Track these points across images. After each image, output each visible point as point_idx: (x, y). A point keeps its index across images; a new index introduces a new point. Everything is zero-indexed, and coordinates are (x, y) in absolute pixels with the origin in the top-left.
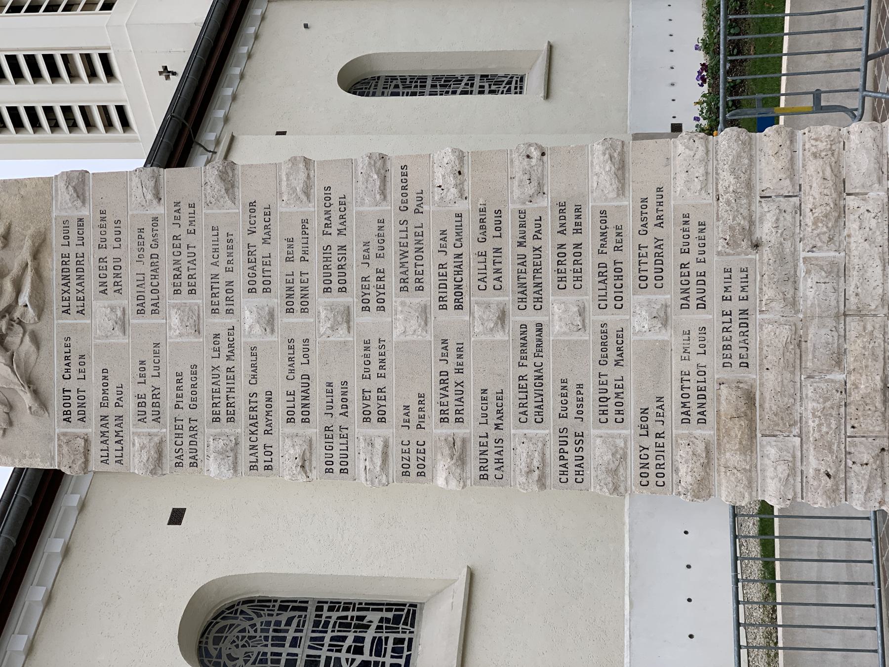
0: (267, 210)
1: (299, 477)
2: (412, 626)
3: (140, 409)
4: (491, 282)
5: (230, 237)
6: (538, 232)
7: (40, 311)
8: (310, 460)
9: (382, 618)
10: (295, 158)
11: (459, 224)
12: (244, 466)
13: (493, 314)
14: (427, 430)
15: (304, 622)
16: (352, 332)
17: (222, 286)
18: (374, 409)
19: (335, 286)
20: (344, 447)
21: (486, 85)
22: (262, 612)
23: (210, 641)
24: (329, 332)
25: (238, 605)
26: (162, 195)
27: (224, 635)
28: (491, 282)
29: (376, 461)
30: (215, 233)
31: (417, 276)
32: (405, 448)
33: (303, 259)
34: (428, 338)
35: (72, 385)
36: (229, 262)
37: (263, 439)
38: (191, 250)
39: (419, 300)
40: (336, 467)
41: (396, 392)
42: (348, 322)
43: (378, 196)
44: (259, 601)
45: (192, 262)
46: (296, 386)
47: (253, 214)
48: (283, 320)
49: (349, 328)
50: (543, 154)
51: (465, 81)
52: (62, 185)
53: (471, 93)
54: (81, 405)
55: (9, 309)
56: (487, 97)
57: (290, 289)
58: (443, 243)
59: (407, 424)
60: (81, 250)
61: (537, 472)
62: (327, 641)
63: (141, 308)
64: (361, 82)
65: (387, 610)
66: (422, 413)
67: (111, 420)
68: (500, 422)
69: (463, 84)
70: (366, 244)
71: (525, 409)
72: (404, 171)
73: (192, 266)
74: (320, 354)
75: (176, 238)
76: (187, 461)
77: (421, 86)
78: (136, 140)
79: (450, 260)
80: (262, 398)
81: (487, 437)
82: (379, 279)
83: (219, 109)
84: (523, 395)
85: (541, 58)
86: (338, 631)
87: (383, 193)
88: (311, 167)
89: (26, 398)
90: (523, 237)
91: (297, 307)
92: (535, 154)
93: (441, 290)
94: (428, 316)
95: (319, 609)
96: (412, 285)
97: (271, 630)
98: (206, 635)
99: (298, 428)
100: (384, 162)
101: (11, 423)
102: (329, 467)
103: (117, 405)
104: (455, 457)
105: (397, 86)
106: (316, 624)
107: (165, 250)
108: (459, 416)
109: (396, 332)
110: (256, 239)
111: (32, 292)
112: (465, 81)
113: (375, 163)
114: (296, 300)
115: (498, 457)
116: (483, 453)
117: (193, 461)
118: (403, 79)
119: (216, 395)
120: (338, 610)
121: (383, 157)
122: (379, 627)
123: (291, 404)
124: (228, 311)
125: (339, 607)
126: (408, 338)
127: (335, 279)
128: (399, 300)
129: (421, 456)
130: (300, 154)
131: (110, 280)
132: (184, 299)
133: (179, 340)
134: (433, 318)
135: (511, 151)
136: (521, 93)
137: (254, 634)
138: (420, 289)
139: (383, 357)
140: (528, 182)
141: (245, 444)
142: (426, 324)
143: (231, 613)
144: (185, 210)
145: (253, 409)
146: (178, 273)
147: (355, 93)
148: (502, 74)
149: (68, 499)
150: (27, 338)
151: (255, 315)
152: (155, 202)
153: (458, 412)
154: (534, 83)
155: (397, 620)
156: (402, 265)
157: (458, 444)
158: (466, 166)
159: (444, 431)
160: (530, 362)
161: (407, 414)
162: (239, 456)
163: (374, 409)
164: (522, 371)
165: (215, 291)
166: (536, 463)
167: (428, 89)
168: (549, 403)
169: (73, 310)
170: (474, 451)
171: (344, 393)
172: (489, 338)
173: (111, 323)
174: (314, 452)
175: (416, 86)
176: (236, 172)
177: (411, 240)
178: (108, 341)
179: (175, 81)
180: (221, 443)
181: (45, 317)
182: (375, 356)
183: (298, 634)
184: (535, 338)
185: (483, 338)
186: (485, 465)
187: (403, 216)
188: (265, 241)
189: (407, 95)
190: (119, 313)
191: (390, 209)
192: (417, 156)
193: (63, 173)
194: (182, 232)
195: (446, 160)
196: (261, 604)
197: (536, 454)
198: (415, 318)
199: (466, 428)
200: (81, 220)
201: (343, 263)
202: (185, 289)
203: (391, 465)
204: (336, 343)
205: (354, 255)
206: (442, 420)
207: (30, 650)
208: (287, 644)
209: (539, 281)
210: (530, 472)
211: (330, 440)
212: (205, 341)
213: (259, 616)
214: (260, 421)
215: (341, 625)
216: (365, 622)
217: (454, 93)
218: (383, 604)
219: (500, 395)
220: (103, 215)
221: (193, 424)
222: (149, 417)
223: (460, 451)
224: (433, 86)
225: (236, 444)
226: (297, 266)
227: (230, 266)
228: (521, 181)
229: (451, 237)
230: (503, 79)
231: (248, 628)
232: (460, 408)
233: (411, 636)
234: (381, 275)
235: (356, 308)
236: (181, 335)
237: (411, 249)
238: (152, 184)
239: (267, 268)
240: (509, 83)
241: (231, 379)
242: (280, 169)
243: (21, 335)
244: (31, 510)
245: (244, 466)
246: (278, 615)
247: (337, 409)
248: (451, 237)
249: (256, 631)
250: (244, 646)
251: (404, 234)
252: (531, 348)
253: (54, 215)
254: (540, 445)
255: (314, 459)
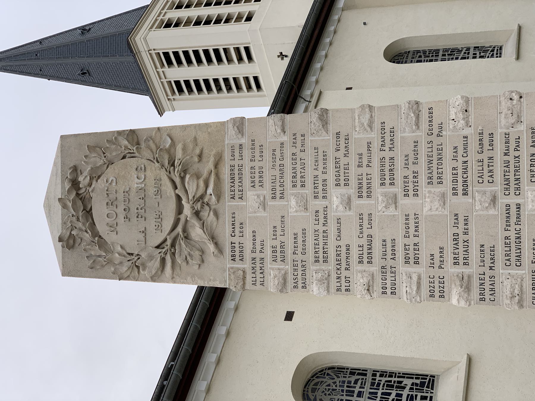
0: (347, 137)
1: (366, 296)
2: (432, 389)
3: (274, 254)
4: (486, 178)
5: (325, 153)
6: (518, 146)
7: (219, 197)
8: (373, 286)
9: (413, 383)
10: (363, 105)
11: (465, 142)
12: (333, 289)
13: (488, 198)
14: (445, 269)
15: (365, 382)
16: (398, 209)
17: (320, 182)
18: (411, 256)
19: (387, 182)
20: (393, 279)
21: (478, 53)
22: (340, 375)
23: (310, 390)
24: (384, 209)
25: (326, 370)
26: (286, 130)
27: (318, 387)
28: (486, 178)
29: (413, 287)
30: (316, 151)
31: (439, 175)
32: (431, 280)
33: (368, 166)
34: (446, 213)
35: (236, 240)
36: (324, 168)
37: (344, 273)
38: (302, 161)
39: (440, 189)
40: (389, 291)
41: (426, 245)
42: (396, 203)
43: (414, 127)
44: (338, 368)
45: (303, 168)
46: (364, 241)
47: (339, 140)
48: (356, 202)
49: (396, 206)
50: (521, 97)
51: (464, 51)
52: (230, 125)
53: (468, 58)
54: (241, 252)
55: (202, 197)
56: (478, 60)
57: (360, 183)
58: (455, 154)
59: (433, 265)
60: (241, 162)
61: (517, 297)
62: (379, 395)
63: (274, 195)
64: (397, 55)
65: (416, 378)
66: (442, 259)
67: (258, 260)
68: (493, 265)
69: (463, 53)
70: (407, 156)
71: (509, 257)
72: (431, 111)
73: (303, 171)
74: (378, 223)
75: (294, 154)
76: (300, 285)
77: (436, 56)
78: (265, 96)
79: (460, 165)
80: (344, 249)
81: (484, 274)
82: (415, 177)
83: (313, 76)
84: (508, 249)
85: (513, 34)
86: (386, 389)
87: (417, 125)
88: (373, 111)
89: (211, 247)
90: (508, 150)
91: (365, 194)
92: (516, 97)
93: (454, 183)
94: (446, 199)
95: (374, 375)
96: (435, 180)
97: (345, 386)
98: (307, 387)
99: (365, 267)
100: (418, 106)
101: (203, 261)
102: (384, 290)
103: (261, 252)
104: (463, 287)
105: (420, 57)
106: (373, 384)
107: (288, 162)
108: (466, 261)
109: (425, 209)
110: (340, 154)
111: (214, 187)
112: (464, 51)
113: (412, 107)
114: (364, 190)
115: (492, 287)
116: (481, 284)
117: (303, 285)
118: (424, 52)
119: (317, 247)
120: (386, 377)
121: (417, 103)
122: (411, 389)
123: (361, 252)
124: (324, 197)
125: (386, 375)
126: (433, 213)
127: (388, 178)
128: (427, 190)
129: (442, 285)
130: (366, 102)
131: (257, 179)
132: (298, 190)
133: (295, 214)
134: (449, 201)
135: (500, 96)
136: (500, 57)
137: (335, 388)
138: (440, 183)
139: (417, 225)
140: (511, 115)
141: (334, 276)
142: (444, 204)
143: (322, 374)
144: (299, 138)
145: (338, 255)
146: (295, 175)
147: (394, 62)
148: (488, 45)
149: (229, 304)
150: (212, 213)
151: (339, 200)
152: (282, 134)
153: (465, 258)
154: (509, 50)
155: (422, 384)
156: (429, 168)
157: (466, 278)
158: (470, 107)
159: (456, 270)
160: (513, 227)
161: (432, 259)
162: (330, 283)
163: (411, 256)
164: (507, 234)
165: (316, 185)
166: (517, 292)
167: (440, 57)
168: (525, 254)
169: (237, 197)
170: (475, 283)
171: (393, 246)
172: (485, 213)
173: (257, 205)
174: (375, 281)
175: (432, 56)
176: (328, 115)
177: (435, 153)
178: (255, 215)
179: (287, 61)
180: (320, 275)
181: (221, 201)
182: (412, 224)
183: (361, 390)
184: (515, 213)
185: (481, 213)
186: (483, 292)
187: (430, 138)
188: (345, 155)
189: (427, 62)
190: (262, 199)
191: (422, 134)
192: (439, 101)
193: (231, 119)
194: (297, 151)
195: (457, 103)
196: (339, 370)
197: (517, 286)
198: (437, 201)
199: (470, 268)
200: (241, 145)
201: (392, 168)
202: (299, 184)
203: (423, 290)
204: (388, 216)
205: (399, 163)
206: (455, 263)
207: (208, 390)
208: (355, 395)
209: (518, 177)
210: (513, 297)
211: (385, 274)
212: (310, 214)
213: (338, 377)
214: (343, 262)
215: (388, 386)
216: (402, 385)
217: (457, 59)
218: (413, 375)
219: (492, 248)
220: (253, 142)
221: (304, 263)
222: (279, 259)
223: (467, 283)
224: (443, 55)
225: (329, 276)
226: (364, 170)
227: (325, 170)
228: (506, 115)
229: (461, 151)
230: (489, 49)
231: (332, 384)
232: (466, 256)
233: (431, 395)
234: (416, 175)
235: (400, 195)
236: (296, 211)
237: (435, 158)
238: (280, 123)
239: (346, 171)
240: (493, 51)
241: (326, 237)
242: (355, 112)
243: (208, 211)
244: (209, 309)
245: (333, 289)
246: (349, 377)
247: (389, 256)
248: (461, 151)
249: (336, 386)
250: (329, 395)
251: (430, 150)
252: (513, 219)
253: (226, 143)
254: (519, 280)
255: (375, 285)
